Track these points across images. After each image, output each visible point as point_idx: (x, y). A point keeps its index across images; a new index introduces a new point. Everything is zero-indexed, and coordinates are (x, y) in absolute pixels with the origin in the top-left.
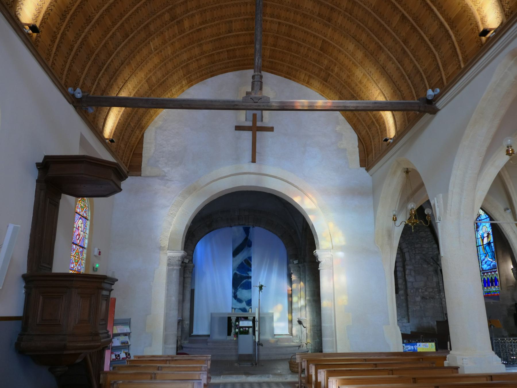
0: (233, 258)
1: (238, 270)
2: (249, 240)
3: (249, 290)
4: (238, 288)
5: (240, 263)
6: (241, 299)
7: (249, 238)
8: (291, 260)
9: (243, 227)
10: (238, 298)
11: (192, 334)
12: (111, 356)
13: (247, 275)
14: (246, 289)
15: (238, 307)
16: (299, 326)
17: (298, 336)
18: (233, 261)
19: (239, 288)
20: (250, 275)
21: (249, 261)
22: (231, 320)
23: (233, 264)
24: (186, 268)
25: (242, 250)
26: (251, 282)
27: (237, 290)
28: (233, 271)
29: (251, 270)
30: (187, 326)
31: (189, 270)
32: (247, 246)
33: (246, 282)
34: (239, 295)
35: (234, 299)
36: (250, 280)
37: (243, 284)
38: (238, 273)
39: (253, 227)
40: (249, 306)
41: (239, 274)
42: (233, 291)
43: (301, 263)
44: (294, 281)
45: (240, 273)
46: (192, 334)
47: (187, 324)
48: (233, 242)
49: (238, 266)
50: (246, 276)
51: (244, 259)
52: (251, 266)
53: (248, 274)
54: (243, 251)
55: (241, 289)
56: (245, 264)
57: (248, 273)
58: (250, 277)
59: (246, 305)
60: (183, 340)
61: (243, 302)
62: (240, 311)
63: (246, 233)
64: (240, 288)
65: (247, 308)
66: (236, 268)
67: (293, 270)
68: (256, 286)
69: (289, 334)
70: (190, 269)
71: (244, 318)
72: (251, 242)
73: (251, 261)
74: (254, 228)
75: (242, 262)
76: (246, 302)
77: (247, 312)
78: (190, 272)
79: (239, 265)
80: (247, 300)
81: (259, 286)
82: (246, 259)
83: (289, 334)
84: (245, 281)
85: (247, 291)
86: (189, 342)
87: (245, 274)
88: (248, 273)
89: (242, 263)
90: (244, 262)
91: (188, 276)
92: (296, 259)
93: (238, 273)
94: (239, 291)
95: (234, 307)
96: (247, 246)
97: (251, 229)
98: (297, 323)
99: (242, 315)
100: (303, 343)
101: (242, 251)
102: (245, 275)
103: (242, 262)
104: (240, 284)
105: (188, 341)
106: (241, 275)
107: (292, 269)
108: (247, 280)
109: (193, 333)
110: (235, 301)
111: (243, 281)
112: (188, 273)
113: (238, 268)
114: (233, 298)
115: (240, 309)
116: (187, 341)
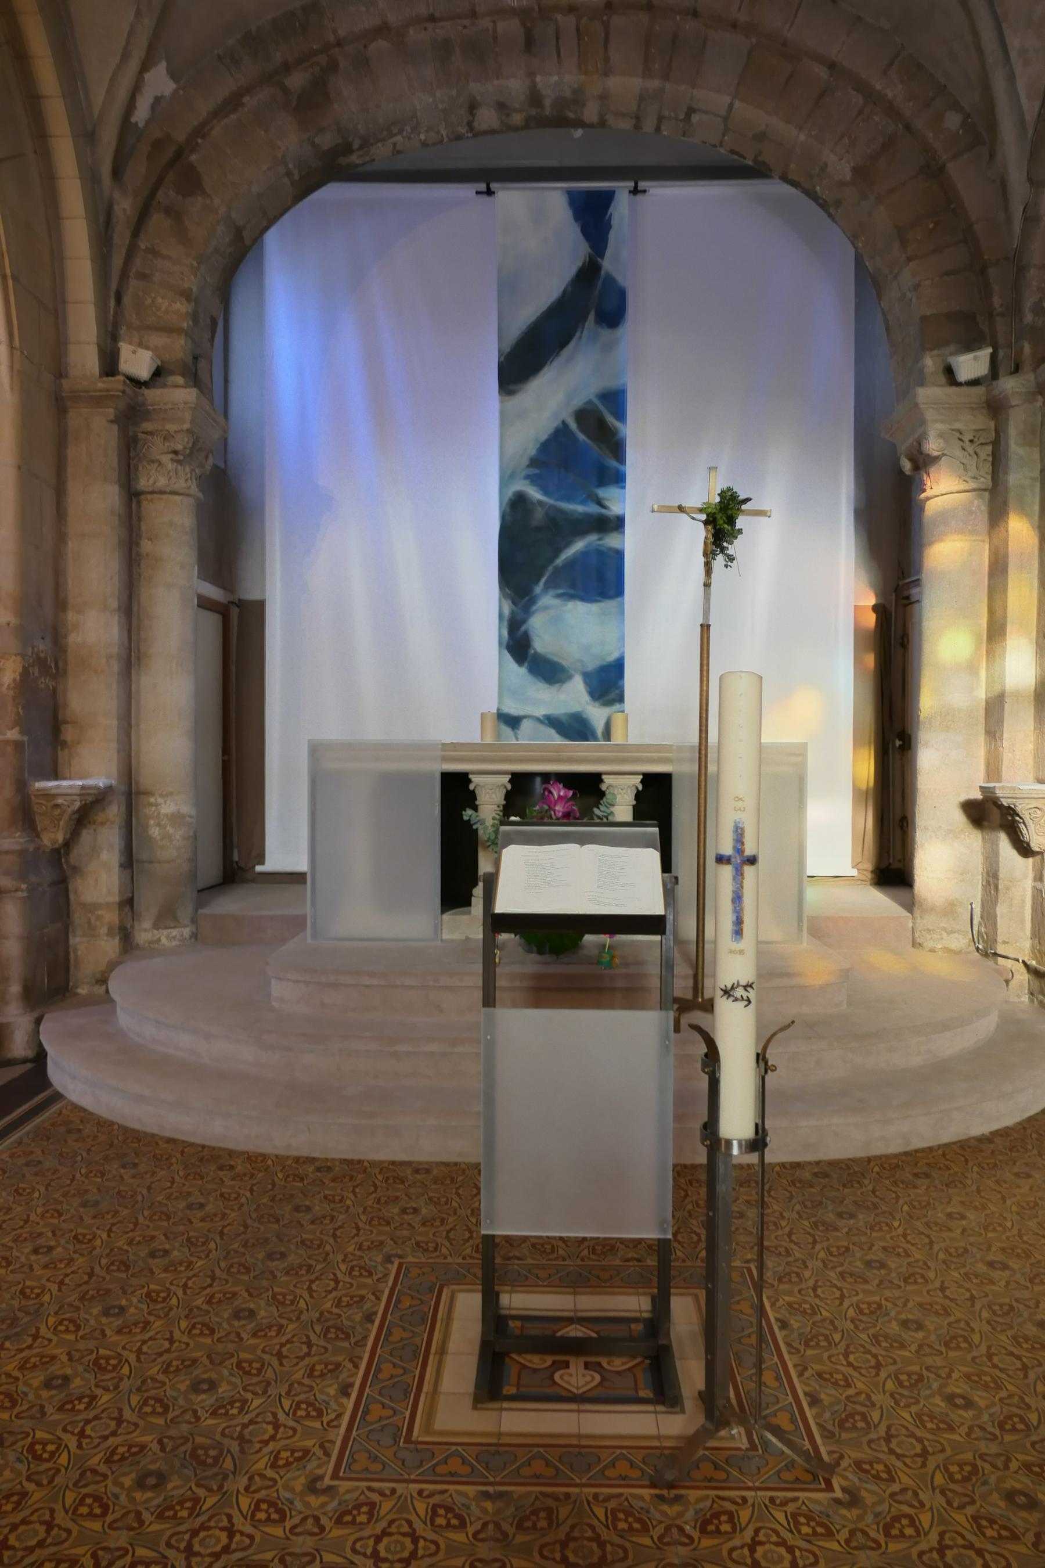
0: (502, 402)
1: (533, 479)
2: (610, 280)
3: (610, 605)
4: (538, 589)
5: (550, 430)
6: (556, 659)
7: (607, 264)
8: (930, 363)
9: (571, 195)
10: (536, 653)
11: (259, 868)
12: (133, 892)
13: (592, 509)
14: (586, 597)
15: (541, 712)
16: (973, 840)
17: (960, 910)
18: (504, 421)
19: (546, 588)
20: (615, 509)
21: (610, 419)
22: (471, 800)
23: (502, 437)
24: (147, 426)
25: (564, 344)
26: (620, 555)
27: (533, 601)
28: (505, 481)
29: (619, 479)
30: (170, 830)
31: (168, 437)
32: (592, 317)
33: (584, 554)
34: (542, 643)
35: (508, 657)
36: (611, 541)
37: (571, 564)
38: (535, 494)
39: (635, 191)
40: (609, 703)
41: (540, 503)
42: (507, 611)
43: (1017, 369)
44: (945, 516)
45: (546, 493)
46: (259, 868)
47: (176, 818)
48: (500, 292)
49: (532, 451)
50: (588, 516)
51: (578, 402)
52: (617, 449)
53: (600, 503)
54: (566, 352)
55: (558, 596)
56: (581, 437)
57: (602, 493)
58: (618, 524)
59: (585, 697)
60: (147, 924)
61: (570, 677)
62: (552, 732)
63: (585, 232)
64: (552, 592)
65: (597, 715)
66: (525, 461)
67: (941, 435)
68: (681, 509)
69: (854, 872)
70: (172, 427)
71: (567, 787)
72: (622, 294)
73: (620, 414)
74: (640, 197)
75: (564, 422)
76: (586, 676)
77: (596, 739)
78: (176, 452)
79: (545, 447)
80: (591, 666)
81: (701, 511)
82: (590, 402)
83: (854, 872)
84: (578, 546)
85: (594, 607)
86: (195, 936)
87: (583, 502)
88: (602, 493)
89: (561, 433)
90: (573, 425)
91: (162, 482)
92: (969, 346)
93: (535, 494)
94: (546, 608)
95: (513, 709)
96: (592, 317)
97: (622, 207)
98: (959, 818)
99: (558, 760)
100: (1009, 964)
101: (558, 354)
102: (580, 508)
103: (564, 422)
104: (550, 569)
105: (187, 932)
106: (551, 507)
107: (939, 426)
108: (592, 538)
109: (262, 862)
110: (518, 673)
111: (568, 544)
112: (166, 459)
113: (533, 462)
114: (506, 652)
115: (552, 722)
116: (174, 932)
